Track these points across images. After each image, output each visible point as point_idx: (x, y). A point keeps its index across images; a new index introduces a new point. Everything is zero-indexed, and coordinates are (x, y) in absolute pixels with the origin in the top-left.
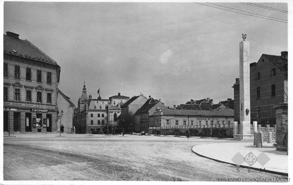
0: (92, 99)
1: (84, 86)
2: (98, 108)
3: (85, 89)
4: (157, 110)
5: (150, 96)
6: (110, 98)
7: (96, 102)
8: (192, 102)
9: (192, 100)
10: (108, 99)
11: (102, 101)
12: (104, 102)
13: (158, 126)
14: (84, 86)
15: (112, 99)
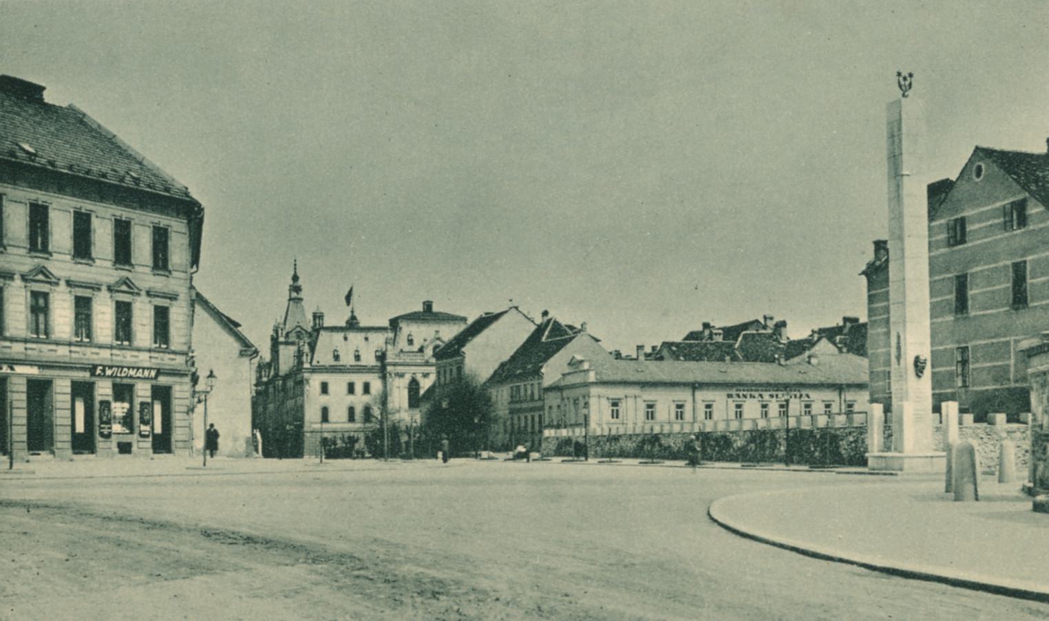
1: (295, 278)
3: (297, 289)
5: (545, 313)
6: (394, 324)
10: (386, 324)
14: (295, 278)
15: (403, 325)
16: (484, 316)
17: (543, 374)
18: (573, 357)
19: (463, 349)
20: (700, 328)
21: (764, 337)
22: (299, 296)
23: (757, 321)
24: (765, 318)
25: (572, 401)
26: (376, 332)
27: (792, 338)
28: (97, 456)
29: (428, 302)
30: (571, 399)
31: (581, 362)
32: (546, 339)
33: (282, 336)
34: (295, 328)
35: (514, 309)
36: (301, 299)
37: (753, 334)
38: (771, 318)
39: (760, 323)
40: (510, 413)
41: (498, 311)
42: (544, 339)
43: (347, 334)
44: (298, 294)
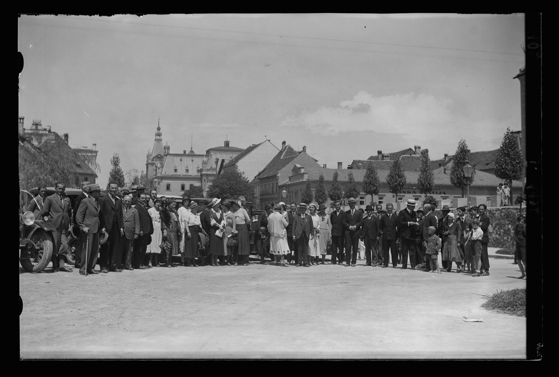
0: (171, 153)
1: (159, 129)
2: (181, 172)
3: (159, 135)
4: (296, 170)
5: (284, 143)
6: (208, 152)
7: (179, 158)
8: (380, 156)
9: (379, 152)
10: (205, 153)
11: (191, 158)
12: (194, 158)
13: (398, 177)
14: (159, 129)
15: (212, 153)
16: (252, 146)
17: (278, 177)
18: (295, 166)
19: (237, 164)
20: (376, 154)
21: (415, 159)
22: (160, 138)
23: (410, 149)
24: (415, 147)
25: (294, 194)
26: (197, 157)
27: (525, 245)
28: (518, 288)
29: (227, 141)
30: (293, 193)
31: (300, 168)
32: (283, 158)
33: (150, 160)
34: (158, 155)
35: (268, 142)
36: (162, 140)
37: (408, 157)
38: (419, 148)
39: (413, 150)
40: (260, 201)
41: (257, 144)
42: (282, 157)
43: (182, 158)
44: (160, 137)
